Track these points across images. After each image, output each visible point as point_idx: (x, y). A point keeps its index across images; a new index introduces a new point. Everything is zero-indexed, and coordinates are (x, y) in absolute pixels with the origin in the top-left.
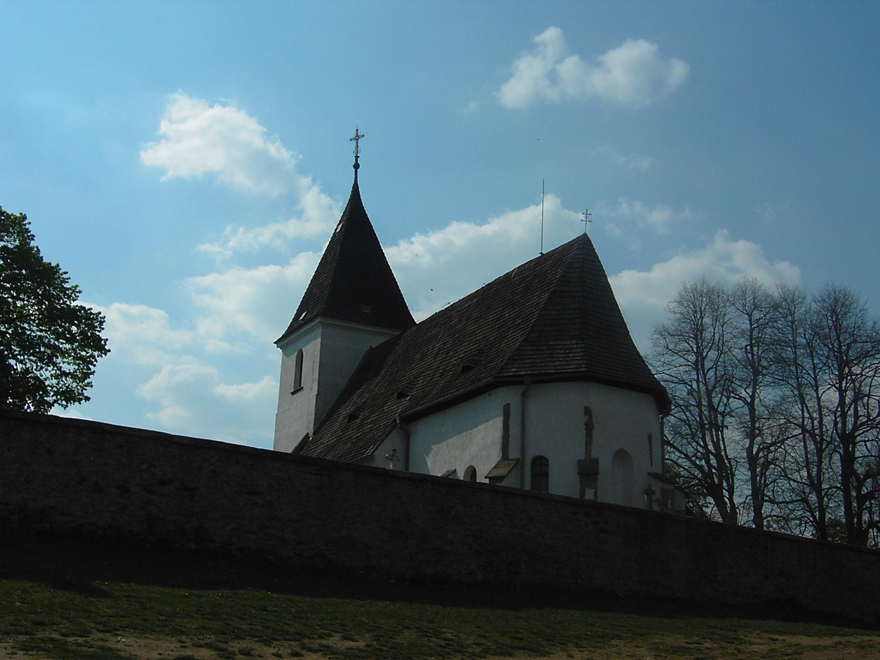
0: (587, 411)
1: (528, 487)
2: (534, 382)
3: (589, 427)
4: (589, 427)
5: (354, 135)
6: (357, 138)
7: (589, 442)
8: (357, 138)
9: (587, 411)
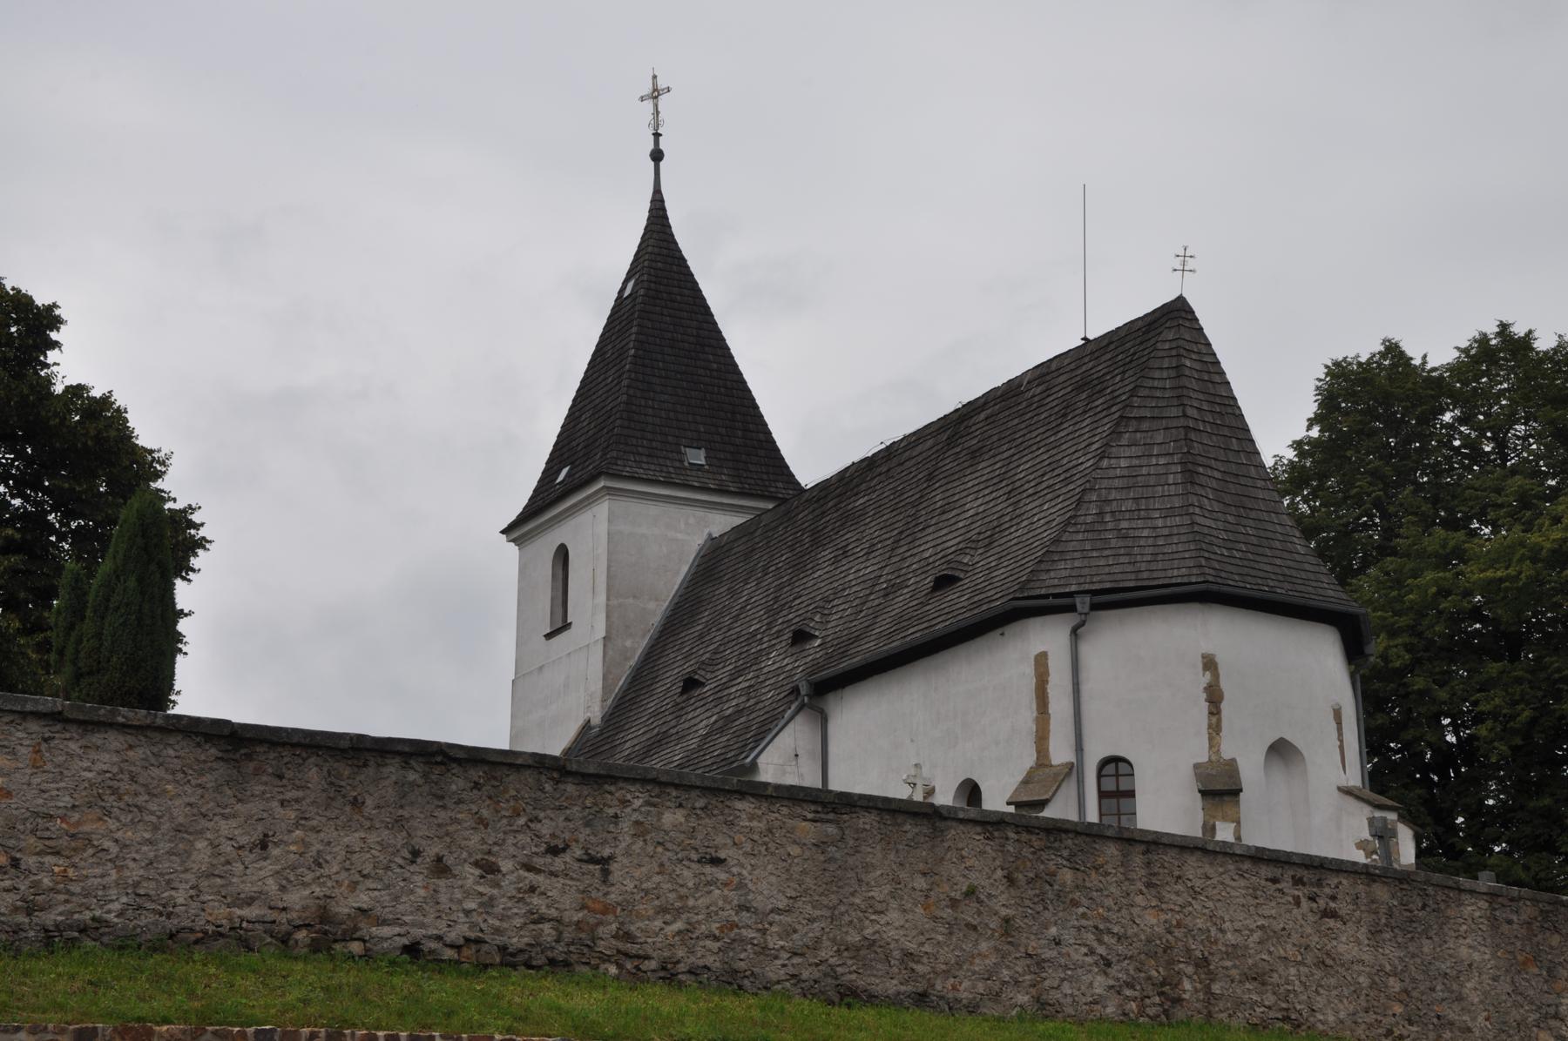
0: (1210, 664)
1: (1092, 816)
2: (1095, 607)
3: (1214, 697)
4: (1214, 697)
5: (647, 89)
6: (655, 94)
7: (1215, 729)
8: (655, 94)
9: (1210, 664)
